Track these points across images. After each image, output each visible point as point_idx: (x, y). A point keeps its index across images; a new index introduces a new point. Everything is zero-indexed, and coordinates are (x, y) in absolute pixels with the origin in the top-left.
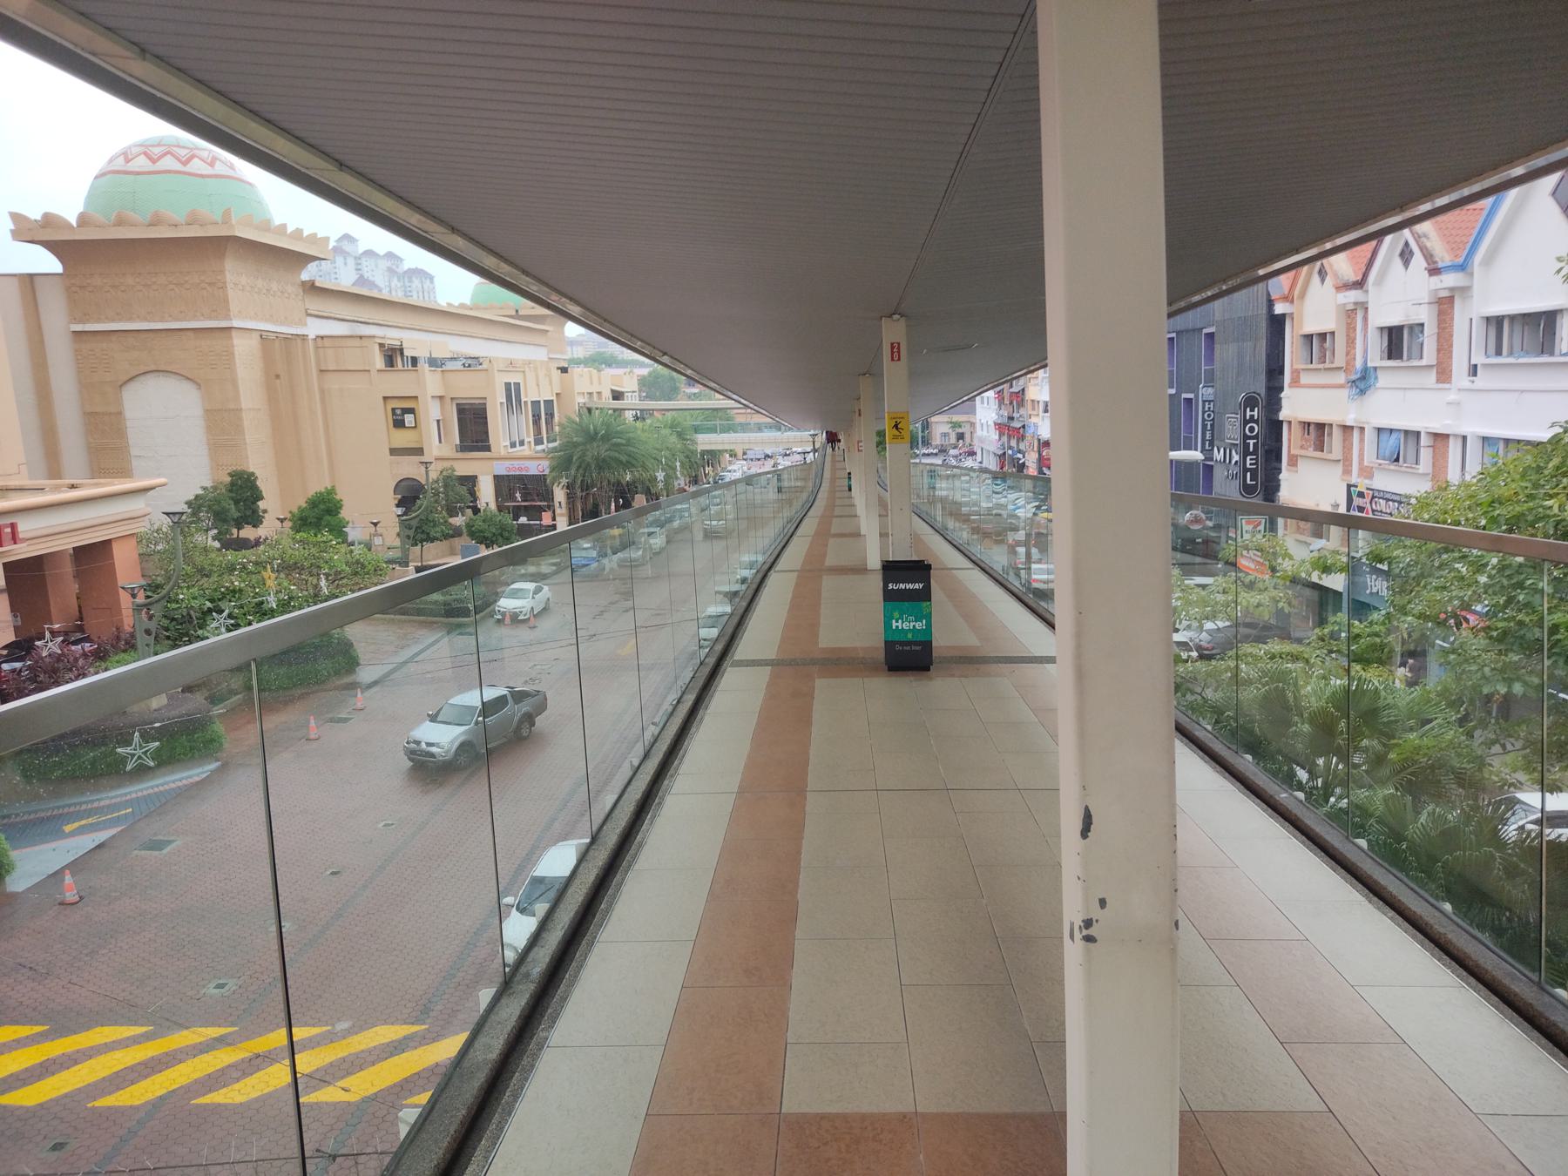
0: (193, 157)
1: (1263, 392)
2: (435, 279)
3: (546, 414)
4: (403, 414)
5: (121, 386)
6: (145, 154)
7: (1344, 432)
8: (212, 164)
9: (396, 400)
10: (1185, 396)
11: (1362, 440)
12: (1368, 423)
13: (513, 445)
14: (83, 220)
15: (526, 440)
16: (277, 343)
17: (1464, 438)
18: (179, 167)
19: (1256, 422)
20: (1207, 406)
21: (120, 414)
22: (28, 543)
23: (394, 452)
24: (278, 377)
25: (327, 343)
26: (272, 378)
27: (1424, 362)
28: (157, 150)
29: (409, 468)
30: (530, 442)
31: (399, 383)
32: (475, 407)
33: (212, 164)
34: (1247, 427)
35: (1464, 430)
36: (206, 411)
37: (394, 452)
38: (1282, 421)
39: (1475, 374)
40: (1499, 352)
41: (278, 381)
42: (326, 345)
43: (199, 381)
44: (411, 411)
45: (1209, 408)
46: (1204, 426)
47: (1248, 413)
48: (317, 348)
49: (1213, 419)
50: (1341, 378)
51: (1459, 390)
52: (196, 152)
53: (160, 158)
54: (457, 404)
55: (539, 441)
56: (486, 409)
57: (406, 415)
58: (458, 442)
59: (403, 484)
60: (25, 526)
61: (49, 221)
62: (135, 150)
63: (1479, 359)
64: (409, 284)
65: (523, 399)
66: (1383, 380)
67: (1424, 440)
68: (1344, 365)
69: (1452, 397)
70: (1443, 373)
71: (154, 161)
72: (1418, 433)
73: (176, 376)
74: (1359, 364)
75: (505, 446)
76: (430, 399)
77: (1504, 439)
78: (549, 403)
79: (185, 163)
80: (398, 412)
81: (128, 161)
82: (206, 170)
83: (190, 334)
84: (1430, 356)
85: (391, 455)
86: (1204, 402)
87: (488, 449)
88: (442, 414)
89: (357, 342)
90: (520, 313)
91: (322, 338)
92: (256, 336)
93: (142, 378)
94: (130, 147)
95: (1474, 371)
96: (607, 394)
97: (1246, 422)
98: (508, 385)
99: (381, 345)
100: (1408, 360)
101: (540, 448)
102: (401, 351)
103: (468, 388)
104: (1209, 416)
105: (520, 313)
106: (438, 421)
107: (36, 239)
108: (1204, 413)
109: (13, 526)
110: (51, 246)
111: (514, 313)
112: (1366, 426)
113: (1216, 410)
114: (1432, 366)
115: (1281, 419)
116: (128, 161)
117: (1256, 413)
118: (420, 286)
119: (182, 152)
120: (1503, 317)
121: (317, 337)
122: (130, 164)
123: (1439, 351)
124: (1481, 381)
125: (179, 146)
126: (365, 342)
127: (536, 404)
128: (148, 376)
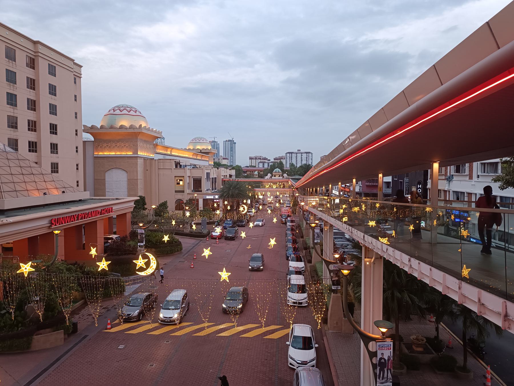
0: (131, 110)
1: (423, 181)
2: (165, 139)
3: (215, 182)
4: (179, 181)
5: (106, 172)
6: (119, 109)
7: (444, 192)
8: (136, 112)
9: (178, 177)
10: (400, 181)
11: (449, 194)
12: (451, 190)
13: (207, 191)
14: (102, 127)
15: (210, 189)
16: (148, 161)
17: (476, 194)
18: (127, 113)
19: (421, 189)
20: (407, 184)
21: (105, 179)
22: (114, 212)
23: (176, 191)
24: (147, 170)
25: (161, 161)
26: (145, 170)
27: (466, 174)
28: (122, 108)
29: (179, 196)
30: (211, 190)
31: (179, 172)
32: (198, 179)
33: (136, 112)
34: (418, 190)
35: (475, 192)
36: (128, 179)
37: (176, 191)
38: (428, 189)
39: (479, 178)
40: (484, 172)
41: (147, 171)
42: (161, 162)
43: (127, 171)
44: (182, 180)
45: (407, 184)
46: (406, 189)
47: (418, 186)
48: (158, 162)
49: (408, 188)
50: (444, 177)
51: (475, 181)
52: (132, 109)
53: (123, 110)
54: (193, 178)
55: (213, 190)
56: (201, 180)
57: (180, 181)
58: (193, 189)
59: (178, 200)
60: (114, 208)
61: (93, 127)
62: (116, 108)
63: (479, 174)
64: (157, 140)
65: (210, 177)
66: (455, 178)
67: (466, 195)
68: (444, 174)
69: (473, 183)
70: (471, 177)
71: (121, 111)
72: (464, 192)
73: (121, 170)
74: (448, 175)
75: (206, 191)
76: (187, 177)
77: (512, 198)
78: (215, 178)
79: (129, 112)
80: (178, 180)
81: (114, 111)
82: (135, 114)
83: (126, 158)
84: (467, 172)
85: (175, 192)
86: (406, 183)
87: (201, 191)
88: (189, 181)
89: (169, 161)
90: (202, 151)
91: (160, 159)
92: (143, 158)
93: (111, 170)
94: (115, 107)
95: (478, 176)
96: (228, 176)
97: (418, 189)
98: (207, 173)
99: (175, 162)
100: (461, 173)
101: (213, 191)
102: (179, 163)
103: (197, 174)
104: (407, 186)
105: (202, 151)
106: (188, 183)
107: (89, 132)
108: (406, 185)
109: (112, 207)
110: (91, 134)
111: (200, 151)
112: (450, 190)
113: (409, 185)
114: (468, 175)
115: (427, 188)
116: (114, 111)
117: (420, 186)
118: (160, 141)
119: (128, 109)
120: (459, 192)
121: (158, 159)
122: (115, 112)
123: (469, 171)
124: (480, 179)
125: (127, 107)
126: (171, 161)
127: (213, 178)
128: (113, 169)
